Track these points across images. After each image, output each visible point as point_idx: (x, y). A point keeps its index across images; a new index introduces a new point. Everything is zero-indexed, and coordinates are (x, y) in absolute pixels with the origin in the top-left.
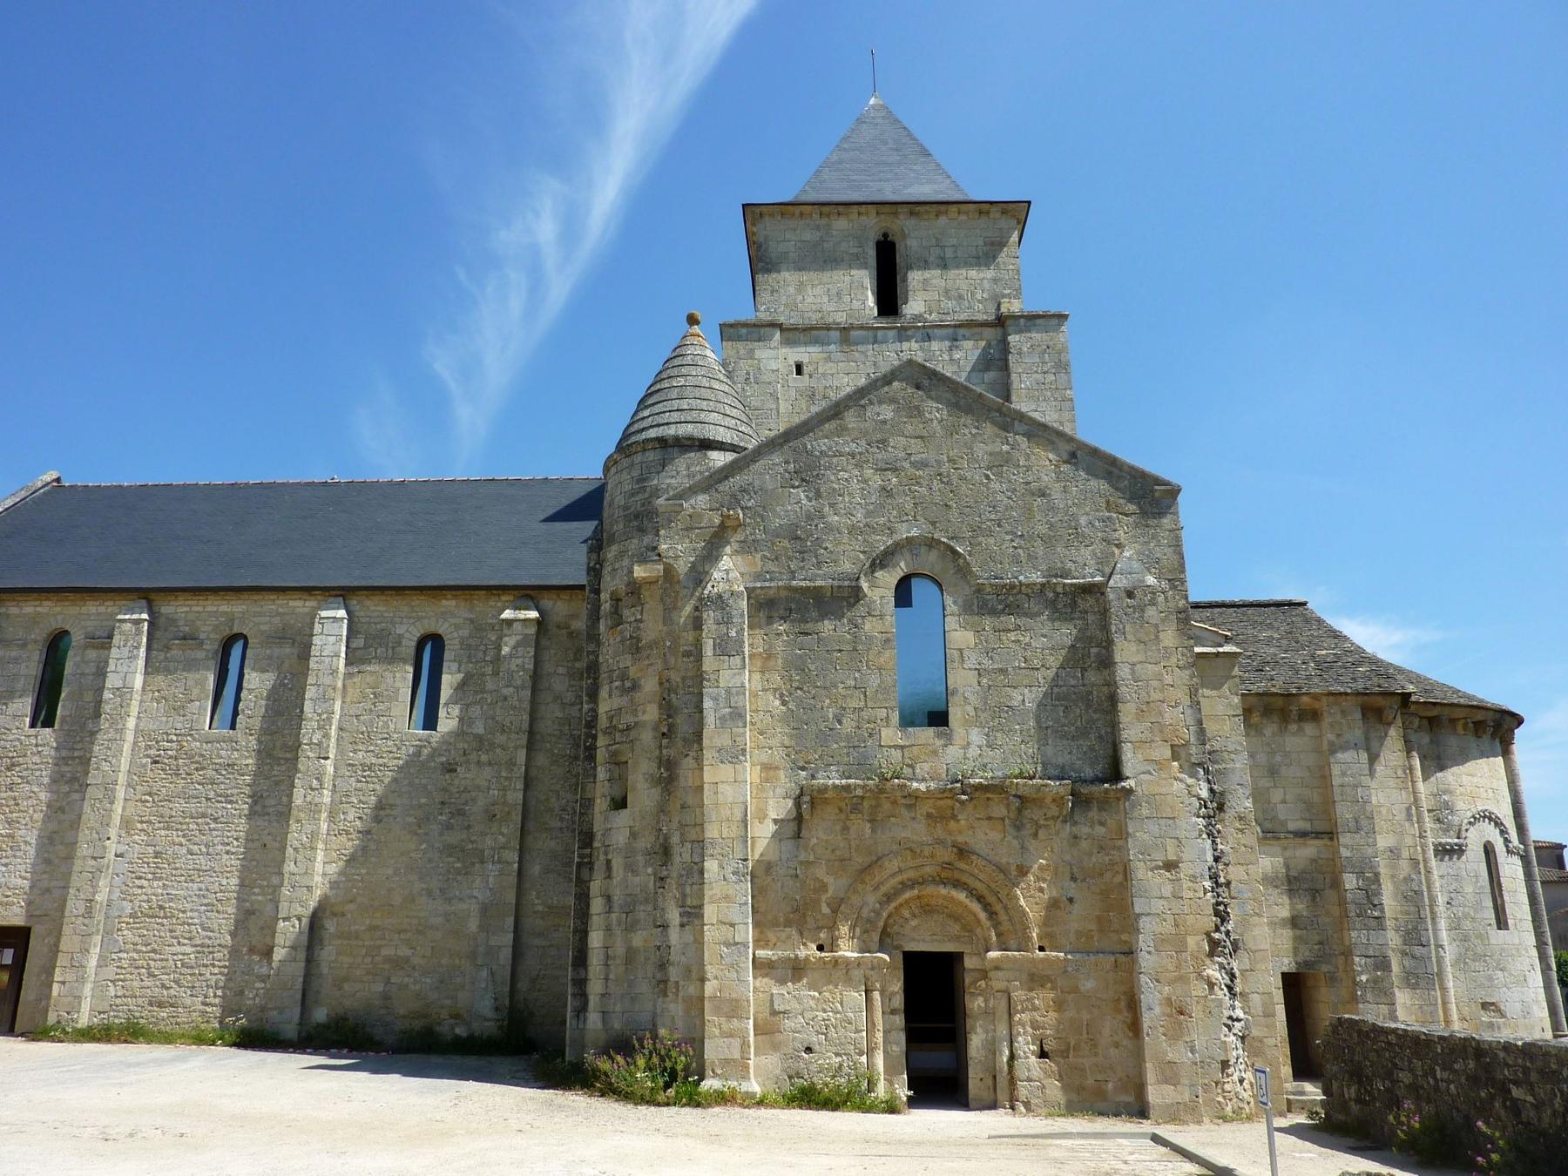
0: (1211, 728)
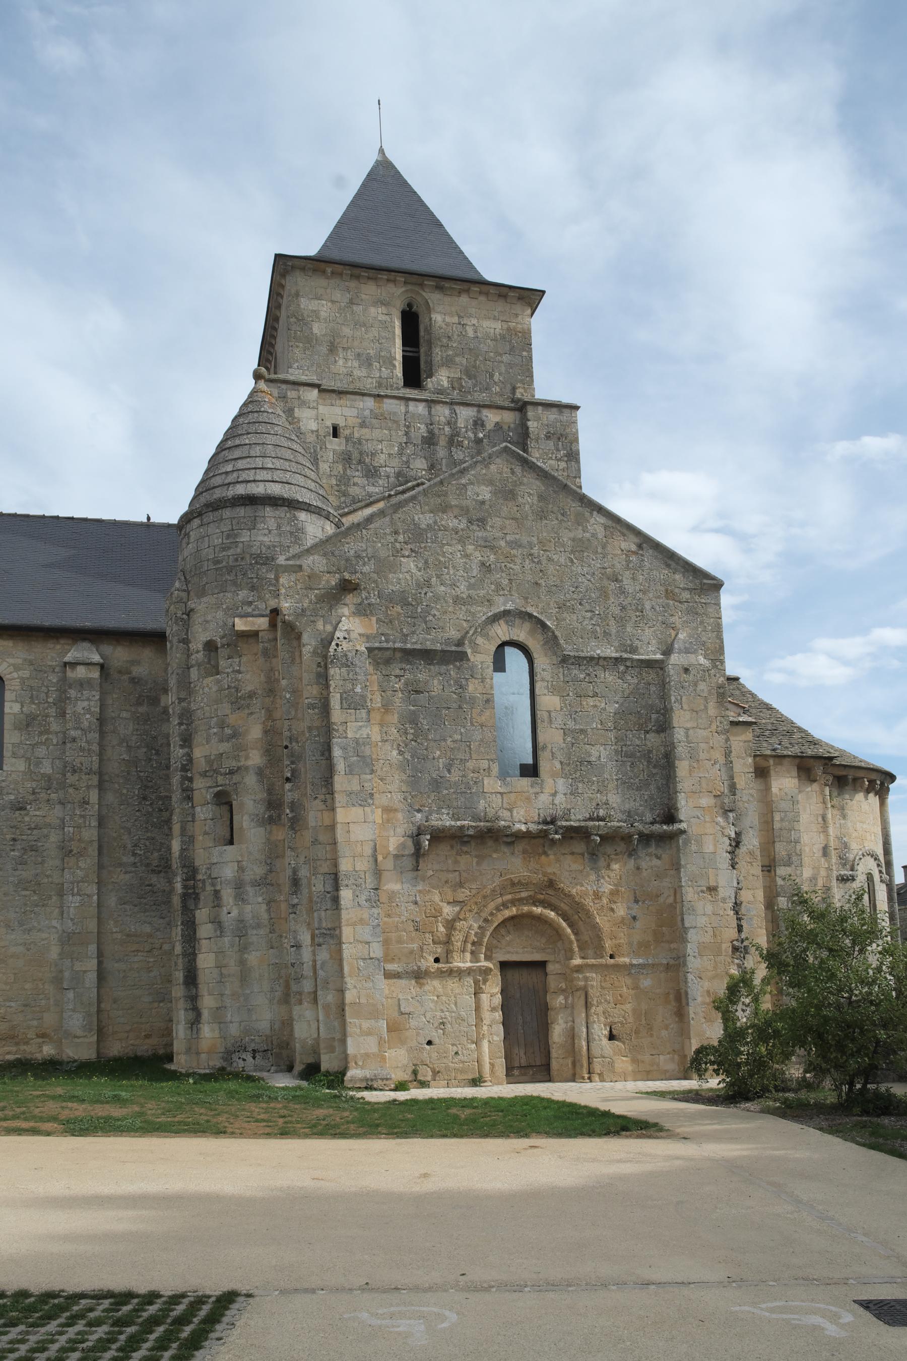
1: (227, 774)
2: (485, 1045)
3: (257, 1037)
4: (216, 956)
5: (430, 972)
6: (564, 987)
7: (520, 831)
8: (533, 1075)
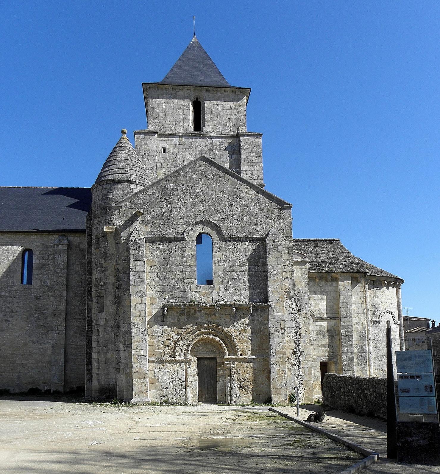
0: (297, 285)
2: (189, 390)
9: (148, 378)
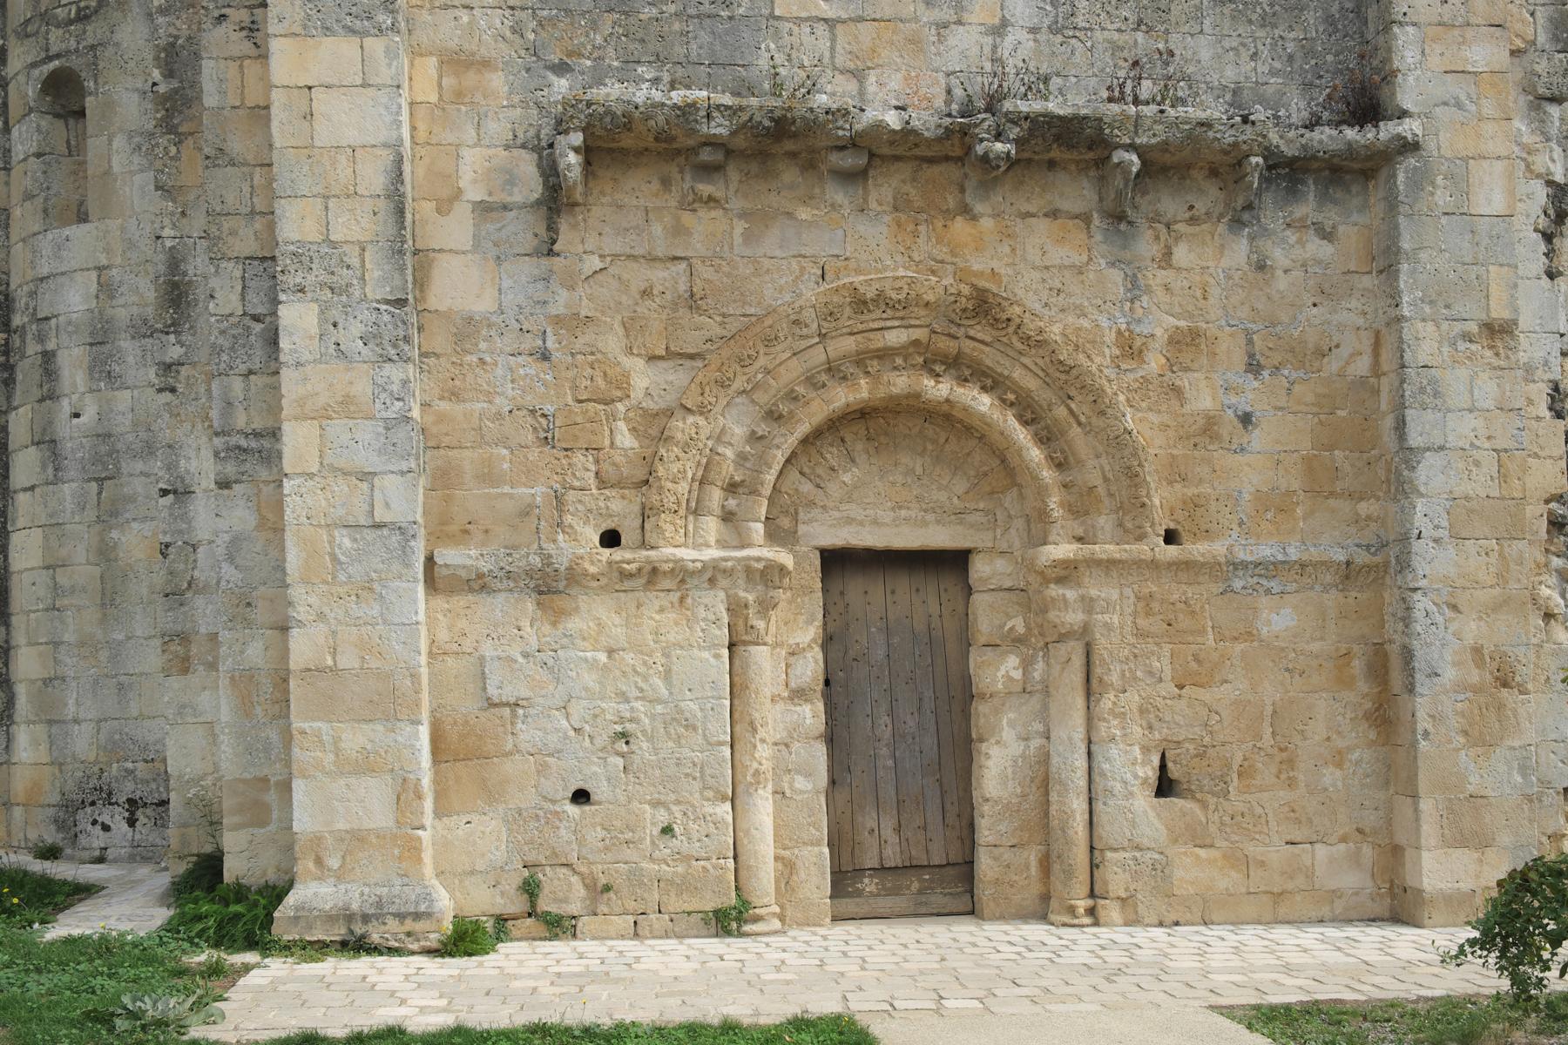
1: (71, 22)
2: (763, 810)
3: (140, 765)
4: (46, 538)
5: (585, 574)
6: (1021, 629)
7: (879, 126)
8: (920, 892)
9: (425, 716)
